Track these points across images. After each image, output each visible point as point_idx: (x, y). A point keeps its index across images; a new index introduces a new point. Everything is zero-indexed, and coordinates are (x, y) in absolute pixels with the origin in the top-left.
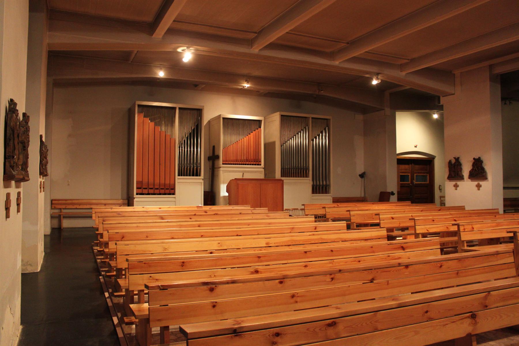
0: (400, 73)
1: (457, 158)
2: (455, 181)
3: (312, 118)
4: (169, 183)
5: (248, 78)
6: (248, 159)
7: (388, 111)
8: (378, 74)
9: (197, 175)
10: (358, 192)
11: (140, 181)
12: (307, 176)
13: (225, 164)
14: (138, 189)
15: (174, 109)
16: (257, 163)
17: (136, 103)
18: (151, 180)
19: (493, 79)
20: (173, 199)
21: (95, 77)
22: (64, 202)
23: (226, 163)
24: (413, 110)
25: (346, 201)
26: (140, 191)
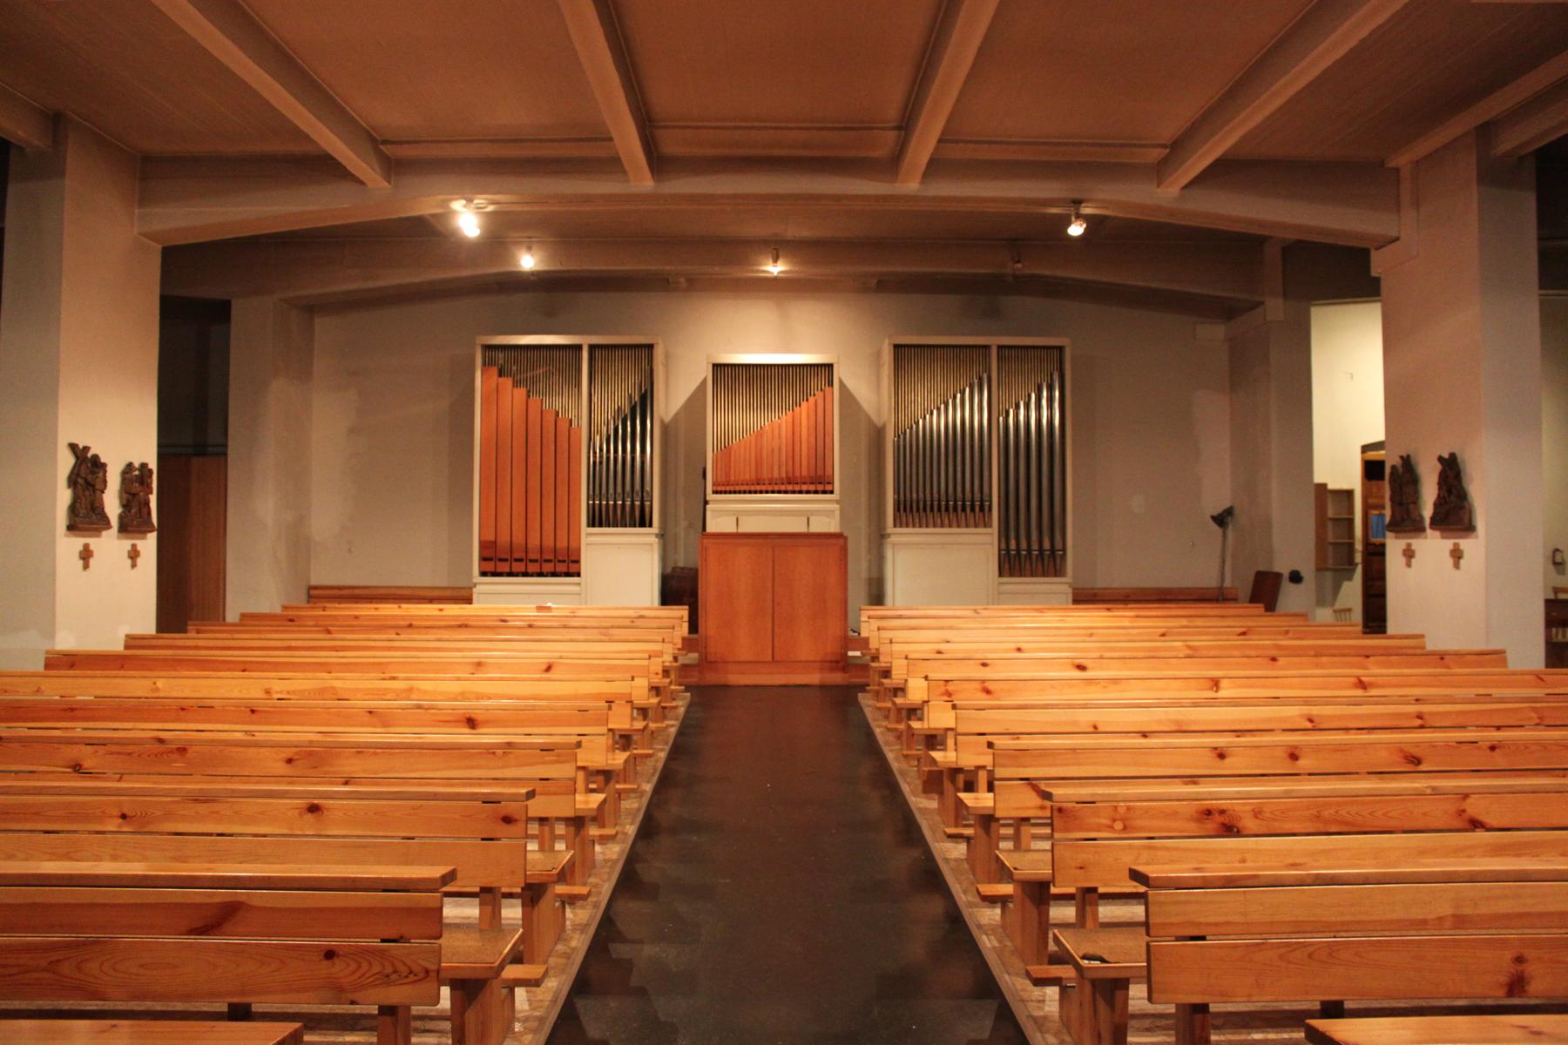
0: (1159, 190)
2: (1403, 538)
3: (1000, 347)
4: (566, 544)
5: (777, 248)
6: (791, 475)
7: (1275, 308)
9: (642, 524)
10: (1205, 575)
11: (490, 542)
13: (721, 492)
14: (484, 562)
15: (579, 348)
17: (477, 342)
18: (519, 539)
19: (1495, 175)
20: (576, 588)
21: (370, 284)
23: (728, 488)
24: (1334, 298)
26: (490, 567)
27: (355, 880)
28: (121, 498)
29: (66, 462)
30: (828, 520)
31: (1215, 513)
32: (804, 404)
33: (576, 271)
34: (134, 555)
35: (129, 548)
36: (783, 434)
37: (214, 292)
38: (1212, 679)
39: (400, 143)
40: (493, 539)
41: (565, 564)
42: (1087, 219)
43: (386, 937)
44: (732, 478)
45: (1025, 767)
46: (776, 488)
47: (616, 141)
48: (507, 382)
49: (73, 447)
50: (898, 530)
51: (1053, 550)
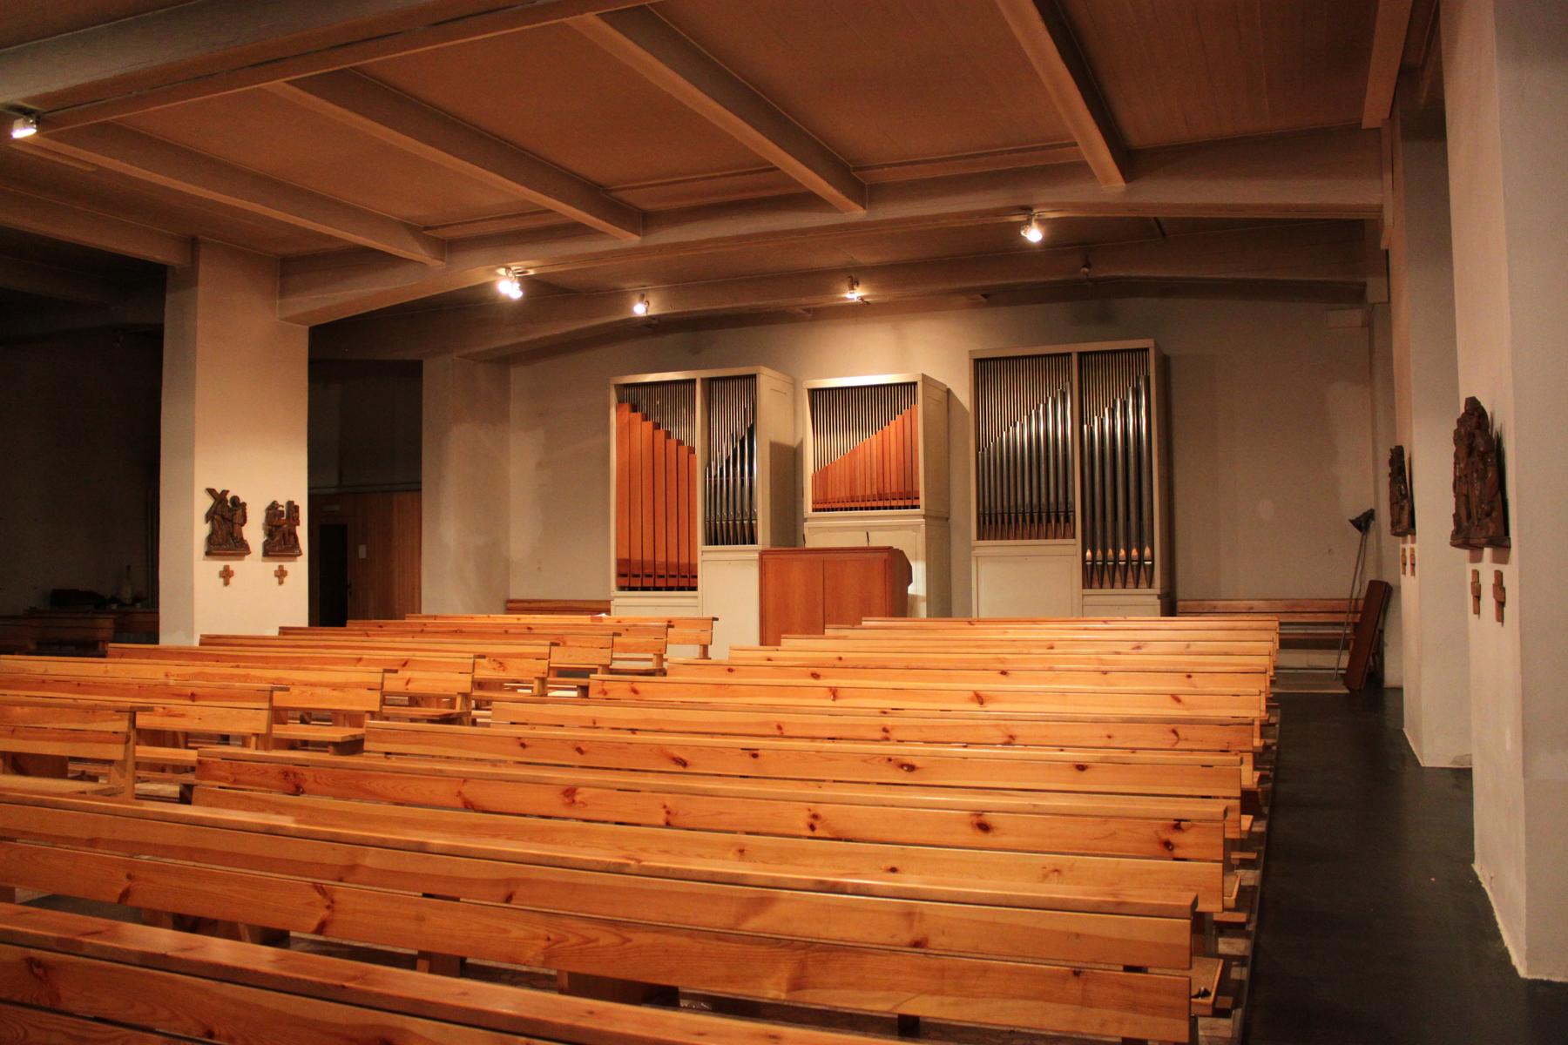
1: (219, 491)
4: (640, 558)
6: (881, 492)
8: (1026, 210)
12: (772, 545)
13: (820, 510)
15: (694, 381)
16: (908, 503)
22: (526, 605)
26: (625, 581)
27: (713, 873)
28: (265, 529)
29: (204, 503)
30: (914, 534)
31: (1354, 516)
32: (892, 422)
33: (689, 313)
34: (281, 574)
35: (277, 569)
36: (875, 452)
37: (409, 355)
38: (830, 688)
39: (436, 228)
40: (628, 557)
41: (683, 579)
42: (1041, 222)
43: (427, 892)
44: (829, 497)
45: (384, 742)
46: (869, 504)
48: (638, 416)
49: (211, 491)
50: (982, 543)
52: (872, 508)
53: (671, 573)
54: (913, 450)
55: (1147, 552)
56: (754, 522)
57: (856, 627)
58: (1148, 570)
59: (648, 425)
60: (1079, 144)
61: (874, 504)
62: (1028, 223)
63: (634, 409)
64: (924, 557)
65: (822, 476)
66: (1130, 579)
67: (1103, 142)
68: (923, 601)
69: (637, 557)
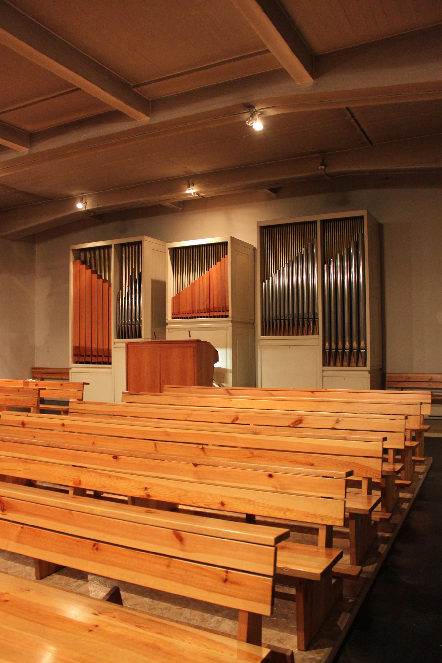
4: (102, 347)
12: (152, 339)
13: (176, 318)
16: (223, 314)
20: (109, 370)
22: (41, 370)
25: (127, 379)
33: (107, 207)
36: (205, 284)
44: (181, 310)
46: (201, 315)
47: (273, 52)
48: (84, 266)
51: (359, 348)
52: (204, 317)
53: (100, 354)
54: (226, 282)
55: (362, 344)
56: (141, 325)
57: (141, 393)
58: (363, 355)
59: (89, 271)
60: (271, 50)
61: (205, 315)
62: (252, 116)
63: (83, 263)
64: (231, 346)
65: (177, 298)
66: (353, 361)
67: (276, 30)
68: (230, 372)
69: (83, 345)
